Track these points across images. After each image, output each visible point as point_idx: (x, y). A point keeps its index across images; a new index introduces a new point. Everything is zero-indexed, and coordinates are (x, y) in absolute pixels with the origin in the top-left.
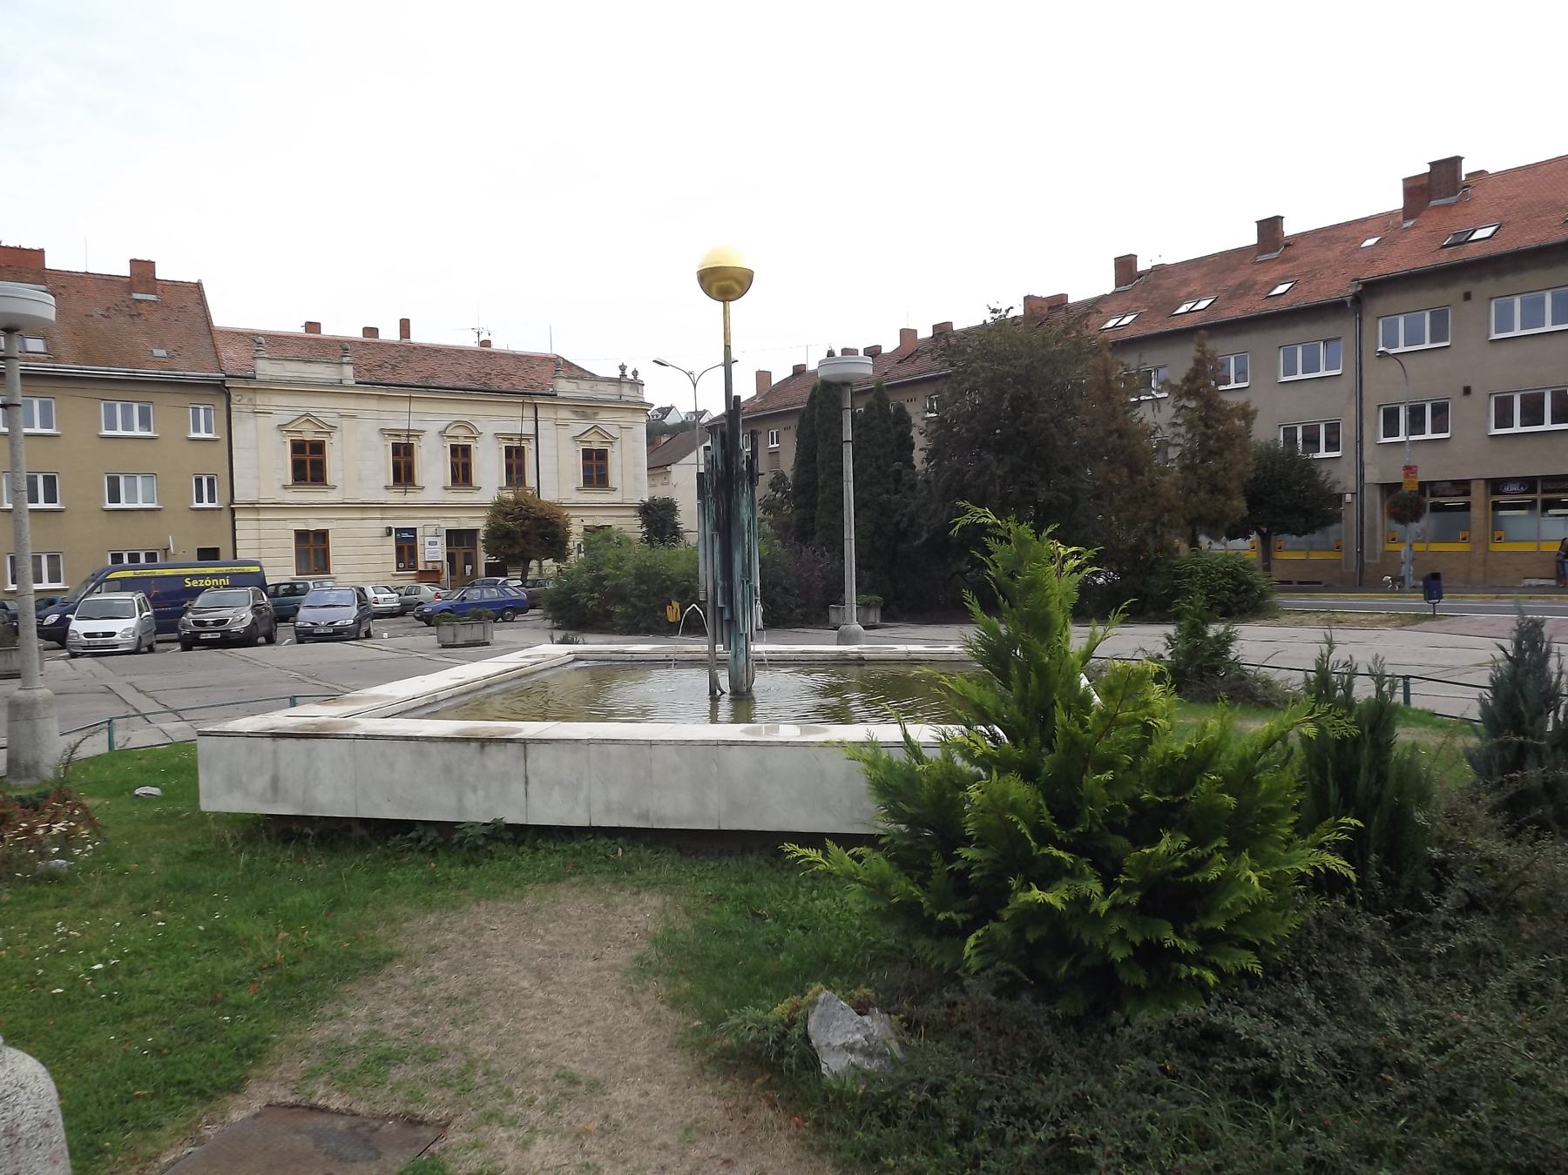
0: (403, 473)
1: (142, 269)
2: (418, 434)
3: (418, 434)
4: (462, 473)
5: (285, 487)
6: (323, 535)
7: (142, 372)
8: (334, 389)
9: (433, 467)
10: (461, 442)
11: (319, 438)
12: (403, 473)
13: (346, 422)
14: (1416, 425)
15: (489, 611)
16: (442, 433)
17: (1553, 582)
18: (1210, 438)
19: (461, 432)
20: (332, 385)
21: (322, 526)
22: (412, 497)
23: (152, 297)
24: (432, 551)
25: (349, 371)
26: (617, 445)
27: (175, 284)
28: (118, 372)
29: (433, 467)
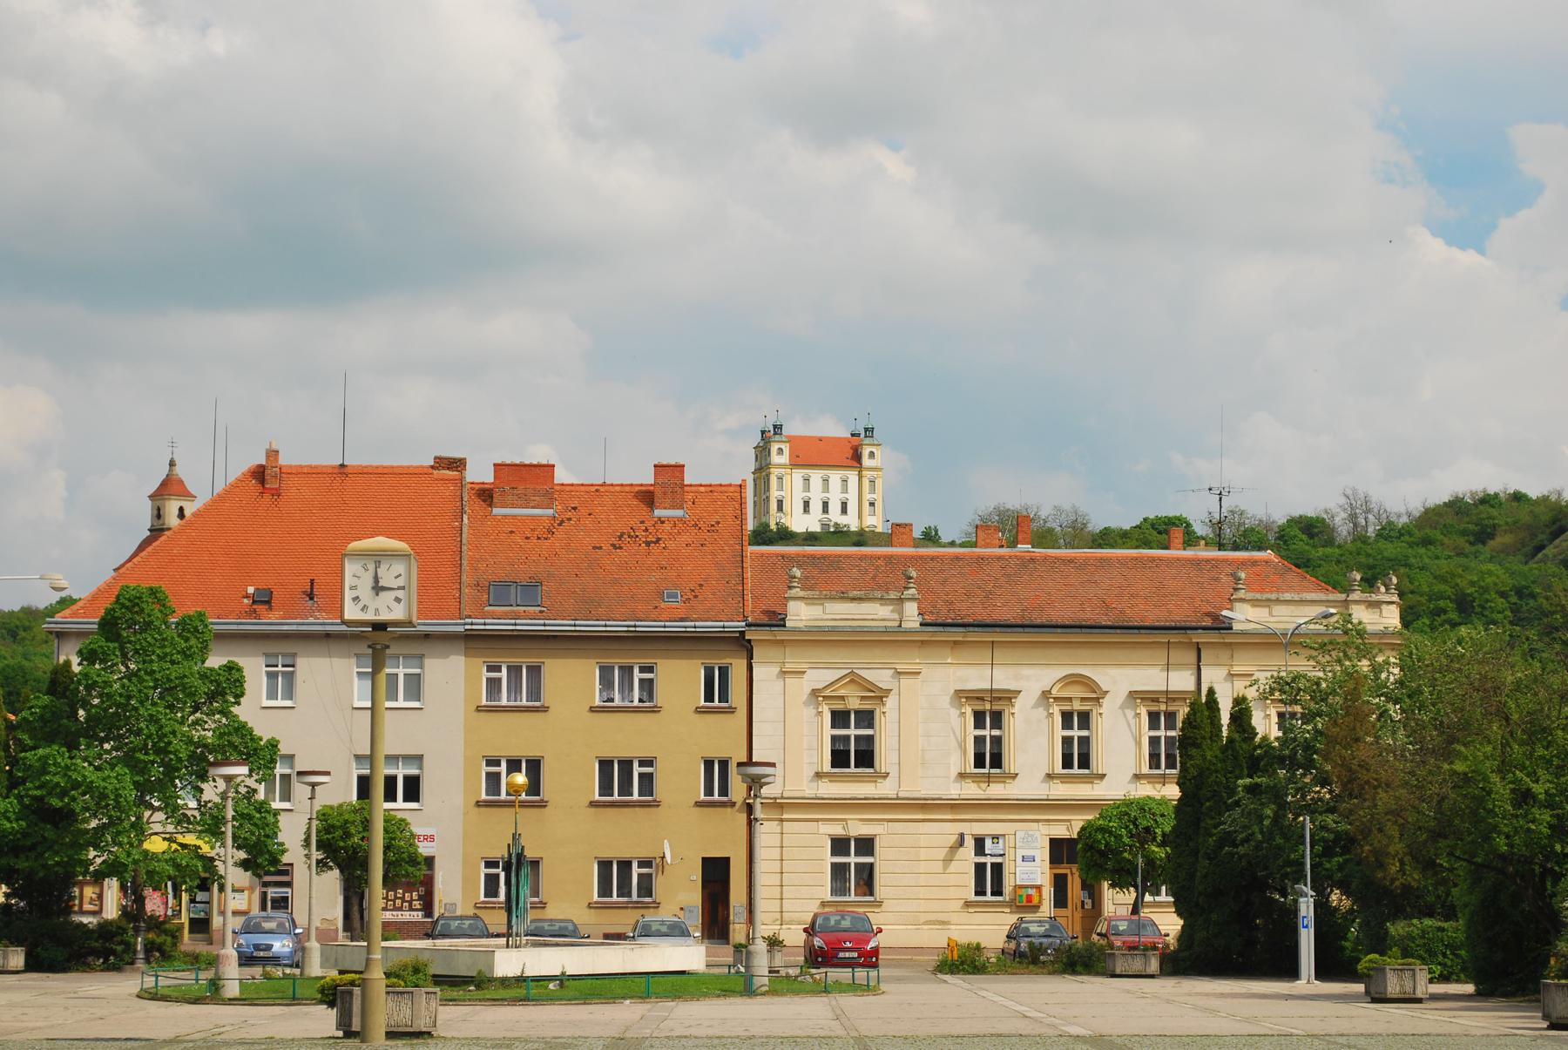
0: (989, 757)
1: (670, 472)
2: (1009, 696)
3: (1009, 696)
4: (1077, 757)
5: (819, 775)
6: (866, 845)
7: (644, 626)
8: (888, 639)
9: (1032, 742)
10: (1077, 706)
11: (867, 706)
12: (989, 757)
13: (905, 682)
14: (391, 782)
15: (355, 901)
16: (1046, 694)
17: (1469, 988)
18: (1150, 861)
19: (1076, 692)
20: (886, 631)
21: (864, 830)
22: (996, 790)
23: (679, 513)
24: (1030, 868)
25: (911, 609)
26: (891, 702)
27: (711, 488)
28: (617, 627)
29: (1032, 742)
